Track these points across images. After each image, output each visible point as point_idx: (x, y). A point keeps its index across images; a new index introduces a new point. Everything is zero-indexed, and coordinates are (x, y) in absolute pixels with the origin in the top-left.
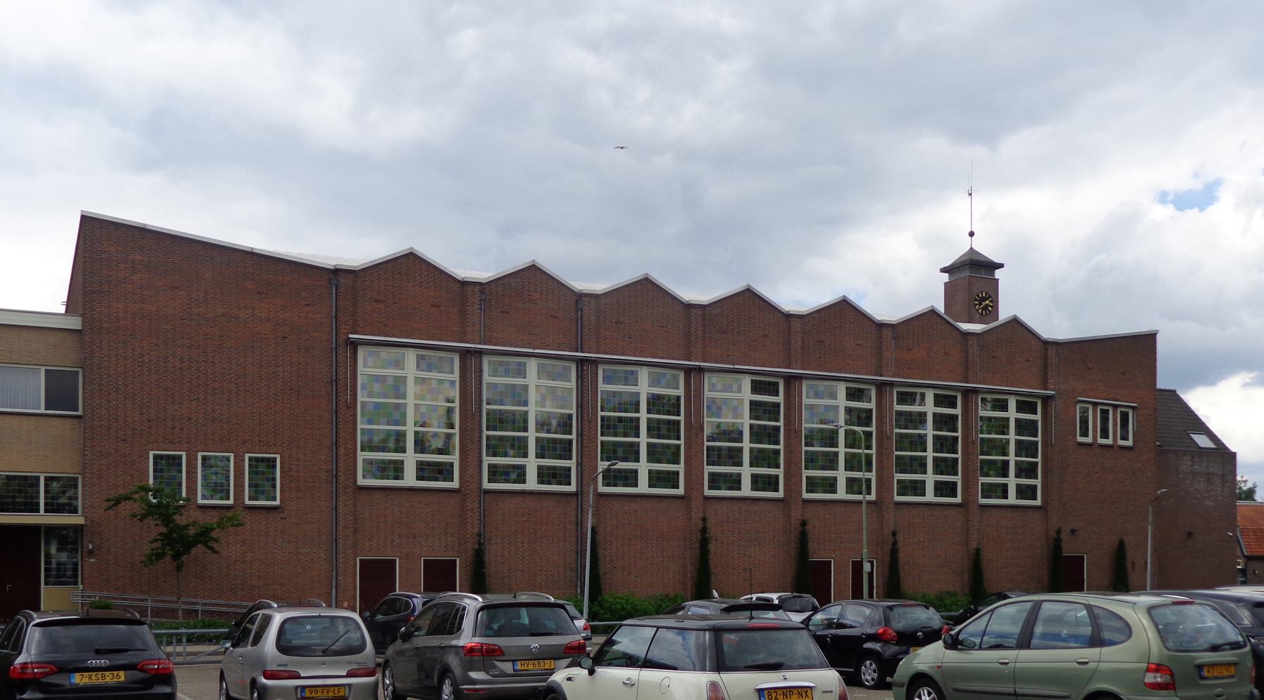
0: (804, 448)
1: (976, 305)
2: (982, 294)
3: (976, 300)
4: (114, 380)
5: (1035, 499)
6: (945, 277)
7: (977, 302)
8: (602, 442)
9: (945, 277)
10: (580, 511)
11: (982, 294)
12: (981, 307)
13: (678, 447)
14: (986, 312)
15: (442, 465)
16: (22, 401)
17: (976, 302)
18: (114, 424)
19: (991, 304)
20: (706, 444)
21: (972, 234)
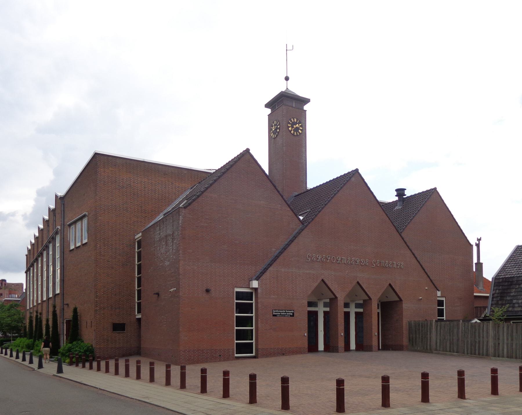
0: (236, 301)
1: (290, 127)
2: (294, 120)
3: (290, 124)
4: (98, 249)
5: (252, 353)
6: (269, 111)
7: (289, 125)
8: (236, 330)
9: (269, 111)
10: (54, 226)
11: (294, 120)
12: (293, 129)
13: (252, 330)
14: (297, 133)
15: (61, 292)
16: (504, 327)
17: (289, 125)
18: (164, 194)
19: (301, 128)
20: (236, 301)
21: (287, 79)
